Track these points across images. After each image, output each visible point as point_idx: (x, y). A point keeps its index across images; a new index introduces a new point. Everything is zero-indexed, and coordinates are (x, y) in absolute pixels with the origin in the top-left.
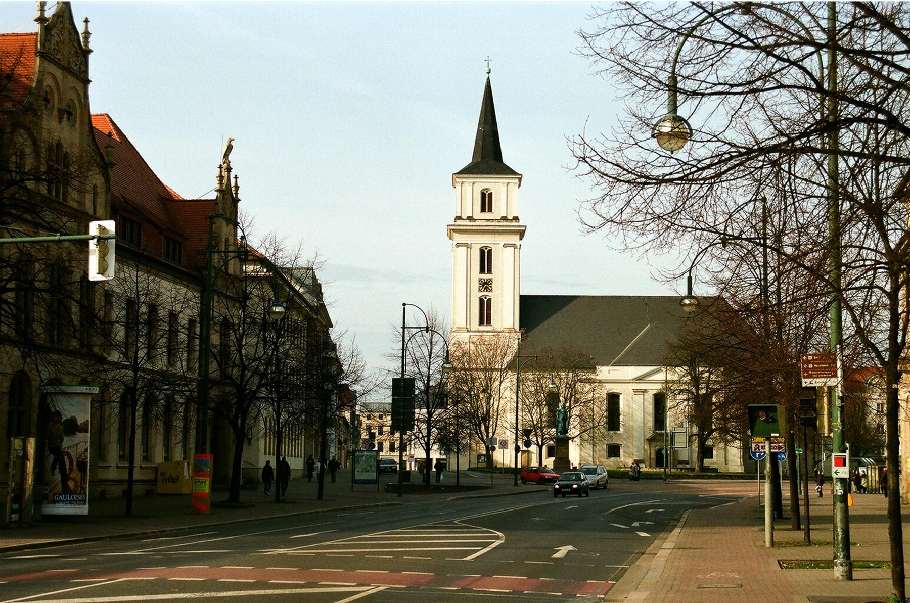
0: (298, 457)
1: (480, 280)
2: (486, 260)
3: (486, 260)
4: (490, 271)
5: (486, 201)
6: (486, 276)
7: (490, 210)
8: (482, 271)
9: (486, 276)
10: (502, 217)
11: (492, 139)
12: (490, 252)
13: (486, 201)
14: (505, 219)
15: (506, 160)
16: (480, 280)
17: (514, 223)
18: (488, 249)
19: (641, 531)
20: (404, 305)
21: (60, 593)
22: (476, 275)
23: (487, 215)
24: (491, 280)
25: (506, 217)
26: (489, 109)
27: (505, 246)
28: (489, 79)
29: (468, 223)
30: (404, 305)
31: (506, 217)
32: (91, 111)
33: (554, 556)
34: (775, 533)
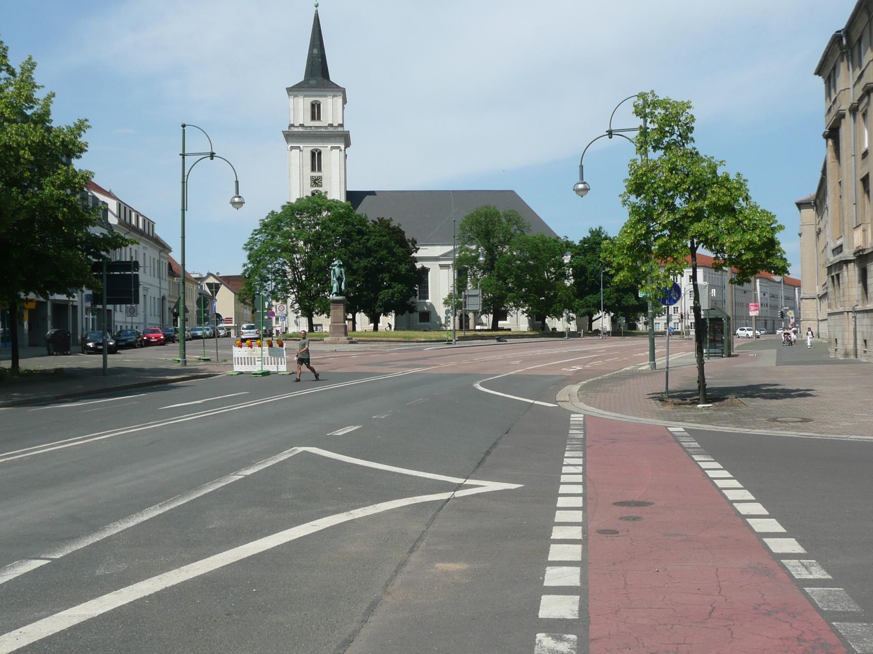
0: (244, 358)
1: (312, 177)
2: (316, 158)
3: (316, 158)
4: (320, 170)
5: (315, 111)
6: (316, 174)
7: (319, 119)
8: (313, 169)
9: (316, 174)
10: (329, 124)
11: (320, 60)
12: (320, 153)
13: (315, 111)
14: (331, 125)
15: (333, 77)
16: (312, 177)
17: (340, 129)
18: (318, 151)
19: (48, 563)
20: (184, 126)
21: (60, 449)
22: (308, 173)
23: (316, 123)
24: (320, 178)
25: (332, 124)
26: (317, 36)
27: (332, 148)
28: (317, 11)
29: (301, 129)
30: (184, 126)
31: (332, 124)
32: (106, 190)
33: (830, 577)
34: (793, 296)
